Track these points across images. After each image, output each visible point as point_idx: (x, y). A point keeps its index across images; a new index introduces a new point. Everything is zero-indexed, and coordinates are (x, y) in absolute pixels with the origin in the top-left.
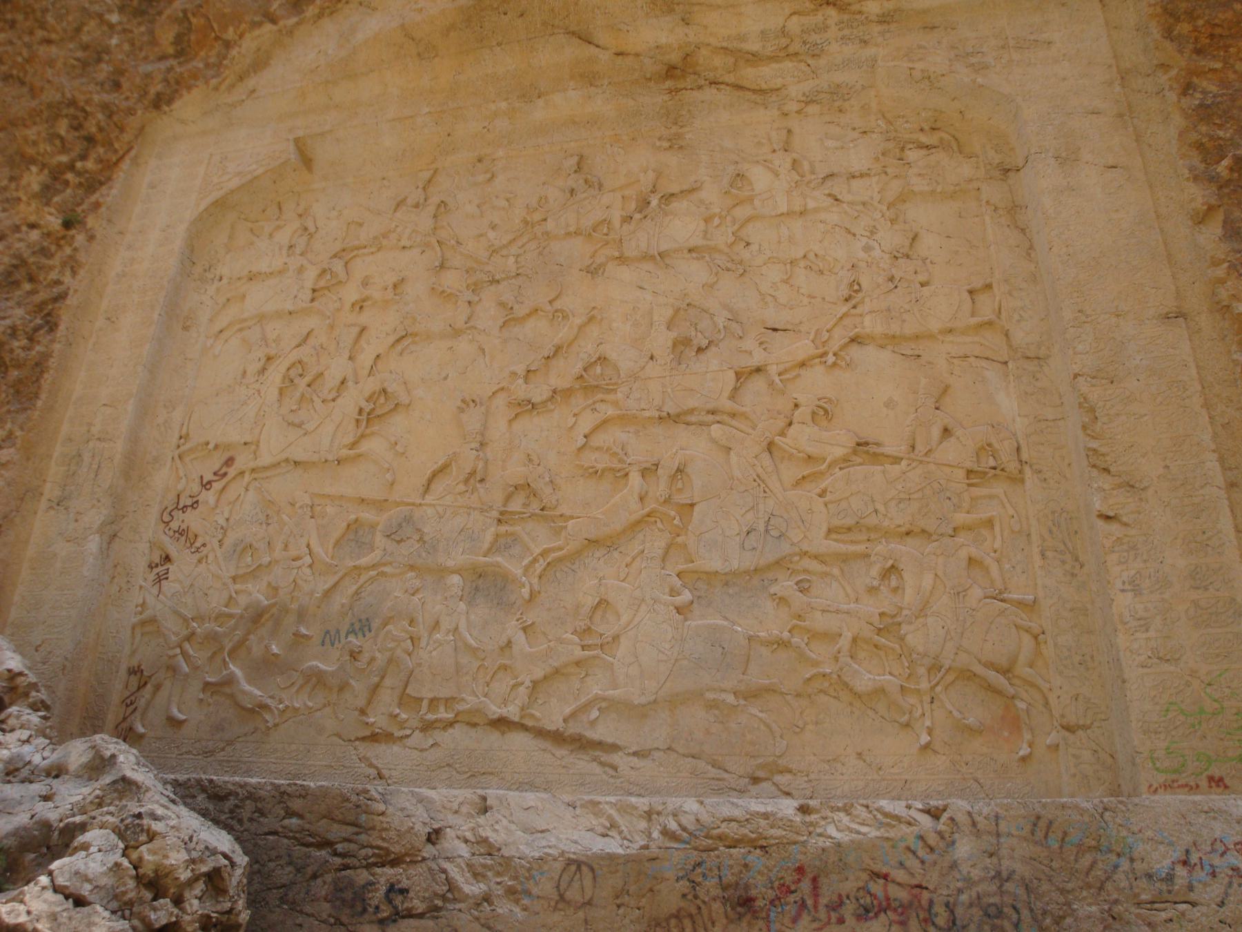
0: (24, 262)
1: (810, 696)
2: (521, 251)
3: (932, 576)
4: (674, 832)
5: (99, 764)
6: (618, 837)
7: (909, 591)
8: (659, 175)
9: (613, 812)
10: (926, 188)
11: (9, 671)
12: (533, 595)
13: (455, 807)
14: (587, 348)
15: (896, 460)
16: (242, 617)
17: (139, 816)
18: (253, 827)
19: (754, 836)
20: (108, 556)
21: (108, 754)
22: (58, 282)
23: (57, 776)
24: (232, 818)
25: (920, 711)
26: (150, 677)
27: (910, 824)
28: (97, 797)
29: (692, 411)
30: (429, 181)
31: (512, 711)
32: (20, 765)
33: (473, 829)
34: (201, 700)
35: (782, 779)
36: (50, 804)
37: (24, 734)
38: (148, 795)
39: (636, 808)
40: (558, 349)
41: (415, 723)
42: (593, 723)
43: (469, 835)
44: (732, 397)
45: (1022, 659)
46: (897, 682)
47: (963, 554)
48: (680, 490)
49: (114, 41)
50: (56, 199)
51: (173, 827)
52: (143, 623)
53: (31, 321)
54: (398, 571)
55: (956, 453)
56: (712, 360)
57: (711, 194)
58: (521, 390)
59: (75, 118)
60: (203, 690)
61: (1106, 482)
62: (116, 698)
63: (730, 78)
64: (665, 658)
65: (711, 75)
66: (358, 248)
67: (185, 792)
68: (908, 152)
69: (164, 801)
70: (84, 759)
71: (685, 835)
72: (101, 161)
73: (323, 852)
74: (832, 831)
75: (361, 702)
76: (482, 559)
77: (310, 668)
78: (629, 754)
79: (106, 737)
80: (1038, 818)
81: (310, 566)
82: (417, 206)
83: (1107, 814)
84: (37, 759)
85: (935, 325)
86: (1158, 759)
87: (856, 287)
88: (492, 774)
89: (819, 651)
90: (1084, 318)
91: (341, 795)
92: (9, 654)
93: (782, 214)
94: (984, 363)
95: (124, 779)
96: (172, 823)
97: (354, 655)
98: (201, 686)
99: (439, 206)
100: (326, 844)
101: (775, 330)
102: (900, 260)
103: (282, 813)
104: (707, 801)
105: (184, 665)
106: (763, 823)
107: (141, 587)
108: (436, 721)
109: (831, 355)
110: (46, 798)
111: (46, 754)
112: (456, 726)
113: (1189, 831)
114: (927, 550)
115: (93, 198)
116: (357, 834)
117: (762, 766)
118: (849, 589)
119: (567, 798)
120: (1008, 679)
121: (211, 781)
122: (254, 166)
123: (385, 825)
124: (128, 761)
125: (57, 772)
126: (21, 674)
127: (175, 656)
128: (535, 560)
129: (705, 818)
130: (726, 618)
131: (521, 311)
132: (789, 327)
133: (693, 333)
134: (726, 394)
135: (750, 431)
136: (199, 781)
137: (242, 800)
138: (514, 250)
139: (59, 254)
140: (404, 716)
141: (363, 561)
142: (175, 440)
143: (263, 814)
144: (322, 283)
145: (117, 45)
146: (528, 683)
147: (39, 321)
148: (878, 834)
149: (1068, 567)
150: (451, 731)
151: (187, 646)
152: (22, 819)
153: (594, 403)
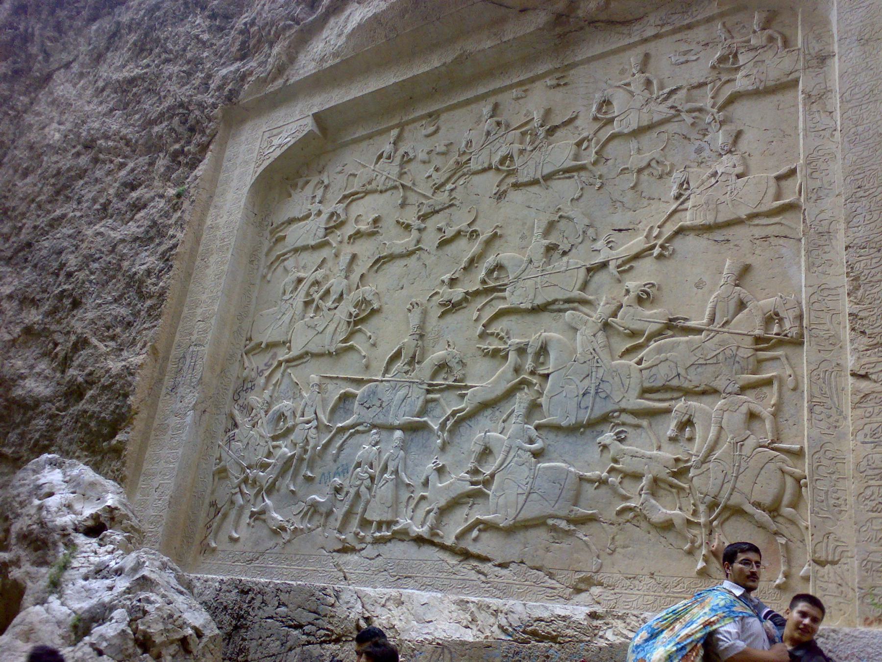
0: (155, 223)
6: (475, 629)
10: (750, 88)
14: (490, 260)
19: (555, 634)
20: (200, 425)
22: (173, 236)
29: (555, 301)
41: (369, 539)
47: (744, 409)
48: (543, 364)
49: (205, 54)
55: (749, 323)
56: (572, 260)
59: (184, 115)
71: (510, 629)
73: (297, 632)
74: (609, 635)
78: (495, 566)
85: (743, 213)
88: (410, 577)
89: (630, 488)
90: (861, 193)
93: (634, 130)
94: (781, 241)
100: (299, 626)
101: (620, 230)
103: (277, 604)
106: (562, 623)
109: (657, 247)
111: (118, 560)
116: (317, 619)
117: (582, 580)
121: (241, 581)
122: (288, 139)
123: (332, 614)
125: (119, 572)
126: (116, 509)
128: (448, 419)
130: (565, 461)
131: (450, 232)
138: (449, 186)
140: (362, 534)
141: (348, 422)
142: (243, 343)
143: (266, 605)
144: (332, 224)
149: (831, 420)
150: (389, 544)
151: (243, 486)
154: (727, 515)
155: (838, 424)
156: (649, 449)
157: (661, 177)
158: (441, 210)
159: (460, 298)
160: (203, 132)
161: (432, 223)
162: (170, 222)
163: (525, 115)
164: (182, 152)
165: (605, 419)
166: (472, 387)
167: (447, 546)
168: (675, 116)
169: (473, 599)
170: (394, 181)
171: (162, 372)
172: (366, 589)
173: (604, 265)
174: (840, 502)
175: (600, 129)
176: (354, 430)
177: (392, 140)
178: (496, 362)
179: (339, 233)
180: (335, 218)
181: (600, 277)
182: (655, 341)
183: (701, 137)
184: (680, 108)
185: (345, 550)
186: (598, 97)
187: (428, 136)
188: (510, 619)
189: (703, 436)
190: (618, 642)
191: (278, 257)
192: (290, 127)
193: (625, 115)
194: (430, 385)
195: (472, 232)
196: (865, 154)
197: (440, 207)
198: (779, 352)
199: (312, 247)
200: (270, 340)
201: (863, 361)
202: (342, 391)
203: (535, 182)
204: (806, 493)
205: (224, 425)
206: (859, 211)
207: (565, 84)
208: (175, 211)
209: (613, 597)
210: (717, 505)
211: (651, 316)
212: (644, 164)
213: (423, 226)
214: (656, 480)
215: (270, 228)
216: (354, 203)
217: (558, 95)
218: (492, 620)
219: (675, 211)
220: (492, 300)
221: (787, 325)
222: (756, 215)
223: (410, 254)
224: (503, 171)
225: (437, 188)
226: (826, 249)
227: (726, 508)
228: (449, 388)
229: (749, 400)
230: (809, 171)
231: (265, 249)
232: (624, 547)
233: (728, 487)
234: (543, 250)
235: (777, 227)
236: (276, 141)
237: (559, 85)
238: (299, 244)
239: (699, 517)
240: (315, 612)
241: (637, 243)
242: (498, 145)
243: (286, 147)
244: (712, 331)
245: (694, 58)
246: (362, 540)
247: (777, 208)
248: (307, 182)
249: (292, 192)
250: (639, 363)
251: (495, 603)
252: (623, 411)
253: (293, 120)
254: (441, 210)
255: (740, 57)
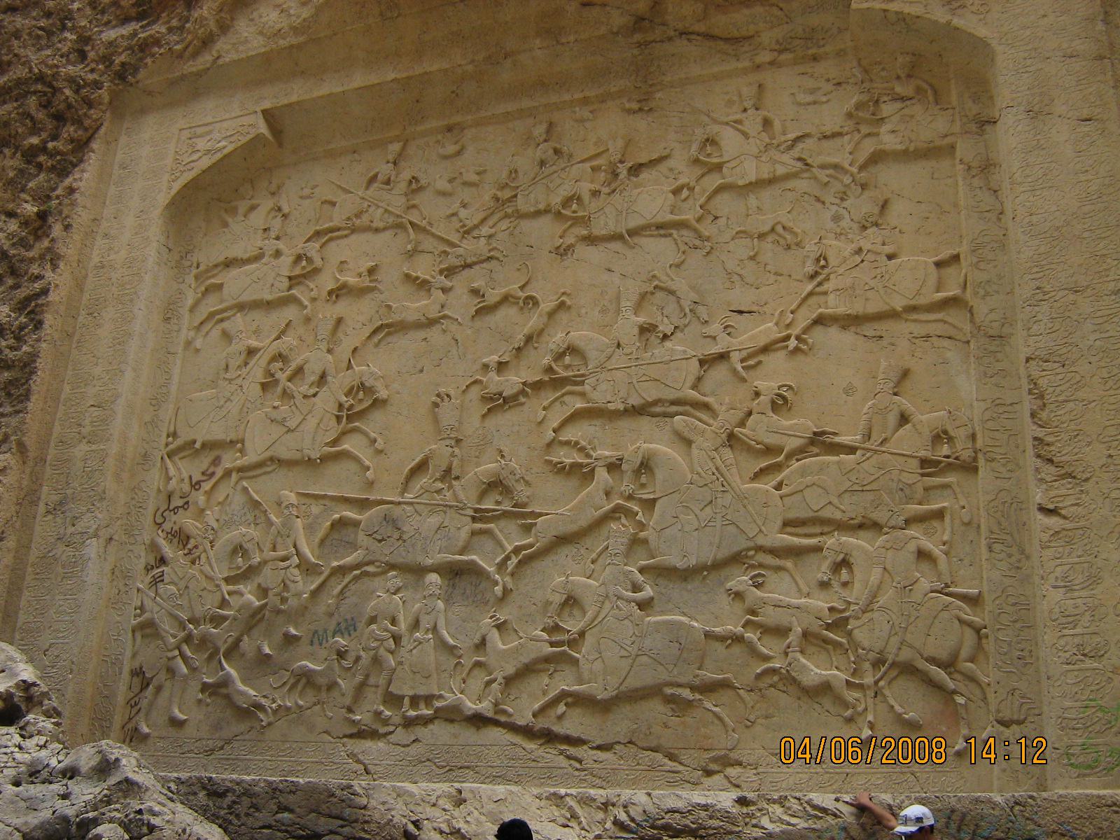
1: (760, 690)
2: (493, 231)
3: (880, 570)
4: (623, 823)
5: (105, 768)
6: (577, 828)
7: (857, 585)
8: (629, 142)
9: (572, 803)
10: (899, 147)
11: (24, 681)
12: (507, 592)
13: (434, 801)
14: (557, 339)
15: (852, 450)
16: (235, 619)
17: (140, 812)
18: (250, 821)
19: (694, 826)
21: (113, 757)
23: (71, 778)
24: (231, 814)
25: (863, 706)
26: (152, 678)
27: (835, 815)
28: (105, 796)
30: (400, 155)
31: (485, 707)
32: (40, 767)
33: (448, 821)
34: (200, 701)
35: (732, 772)
36: (67, 802)
37: (42, 740)
38: (148, 794)
39: (595, 800)
40: (529, 339)
42: (560, 718)
43: (444, 827)
44: (694, 387)
45: (964, 653)
46: (843, 676)
47: (912, 546)
50: (31, 185)
51: (168, 821)
52: (142, 626)
53: (16, 319)
54: (379, 570)
55: (910, 442)
57: (678, 162)
58: (494, 381)
59: (45, 94)
60: (203, 691)
61: (1049, 471)
62: (121, 699)
63: (701, 27)
64: (626, 654)
65: (680, 26)
66: (331, 230)
67: (186, 792)
68: (883, 106)
69: (162, 799)
70: (93, 763)
72: (72, 141)
74: (765, 822)
75: (348, 701)
76: (458, 557)
77: (301, 667)
78: (592, 748)
79: (110, 742)
80: (953, 811)
81: (298, 566)
82: (388, 182)
83: (1017, 808)
84: (54, 762)
85: (898, 304)
86: (1073, 755)
87: (823, 262)
88: (468, 767)
90: (1040, 296)
91: (328, 790)
92: (22, 666)
93: (751, 183)
94: (946, 343)
95: (127, 780)
96: (167, 818)
97: (341, 655)
98: (200, 687)
99: (411, 182)
101: (741, 312)
102: (870, 231)
103: (275, 808)
104: (655, 793)
105: (183, 666)
106: (703, 814)
107: (138, 590)
108: (417, 717)
109: (793, 339)
110: (65, 797)
111: (61, 758)
112: (436, 722)
113: (1091, 823)
114: (877, 544)
115: (68, 181)
116: (342, 826)
118: (801, 582)
119: (536, 791)
120: (949, 674)
121: (210, 779)
122: (223, 143)
124: (130, 764)
125: (71, 773)
126: (34, 684)
127: (174, 657)
128: (508, 558)
129: (651, 809)
130: (684, 614)
131: (493, 296)
132: (755, 308)
133: (659, 318)
134: (689, 384)
135: (711, 421)
136: (199, 779)
137: (238, 796)
138: (485, 230)
139: (37, 245)
140: (388, 713)
141: (349, 560)
142: (163, 439)
143: (258, 810)
144: (298, 271)
145: (79, 9)
146: (500, 680)
147: (23, 319)
148: (806, 825)
149: (1013, 559)
150: (431, 727)
151: (185, 648)
152: (46, 814)
153: (563, 395)
154: (894, 673)
155: (1020, 565)
156: (794, 596)
157: (788, 247)
158: (475, 263)
159: (515, 391)
160: (78, 122)
161: (460, 283)
162: (31, 254)
163: (595, 144)
164: (43, 149)
165: (736, 559)
166: (541, 515)
167: (520, 726)
168: (802, 171)
169: (573, 791)
170: (398, 216)
171: (36, 480)
172: (403, 784)
173: (723, 357)
174: (1026, 653)
175: (703, 176)
176: (359, 571)
177: (391, 158)
178: (573, 482)
179: (312, 285)
180: (304, 263)
181: (719, 373)
182: (798, 460)
183: (838, 201)
184: (809, 161)
185: (361, 734)
186: (700, 134)
187: (446, 157)
188: (632, 813)
189: (865, 577)
190: (777, 830)
191: (211, 315)
192: (225, 125)
193: (738, 161)
194: (476, 510)
195: (527, 298)
196: (1042, 249)
197: (474, 259)
198: (950, 478)
199: (268, 303)
200: (209, 437)
201: (1052, 493)
202: (337, 516)
203: (617, 237)
204: (990, 645)
205: (143, 560)
206: (1040, 317)
207: (651, 110)
208: (38, 238)
209: (754, 778)
210: (883, 663)
211: (791, 427)
212: (767, 228)
213: (449, 284)
214: (805, 634)
215: (194, 271)
216: (333, 244)
217: (641, 124)
218: (601, 815)
219: (811, 294)
220: (563, 395)
221: (959, 445)
222: (913, 309)
223: (431, 323)
224: (567, 218)
225: (468, 232)
226: (999, 356)
227: (893, 664)
228: (506, 514)
229: (918, 537)
230: (975, 260)
231: (190, 302)
232: (767, 717)
233: (895, 641)
234: (636, 331)
235: (940, 325)
236: (202, 144)
237: (641, 110)
238: (247, 297)
239: (861, 678)
240: (337, 818)
241: (766, 330)
242: (559, 181)
243: (219, 156)
244: (868, 450)
245: (824, 99)
246: (386, 722)
247: (942, 300)
248: (253, 208)
249: (230, 220)
250: (778, 487)
251: (599, 794)
252: (760, 549)
253: (227, 116)
254: (475, 263)
255: (883, 106)
